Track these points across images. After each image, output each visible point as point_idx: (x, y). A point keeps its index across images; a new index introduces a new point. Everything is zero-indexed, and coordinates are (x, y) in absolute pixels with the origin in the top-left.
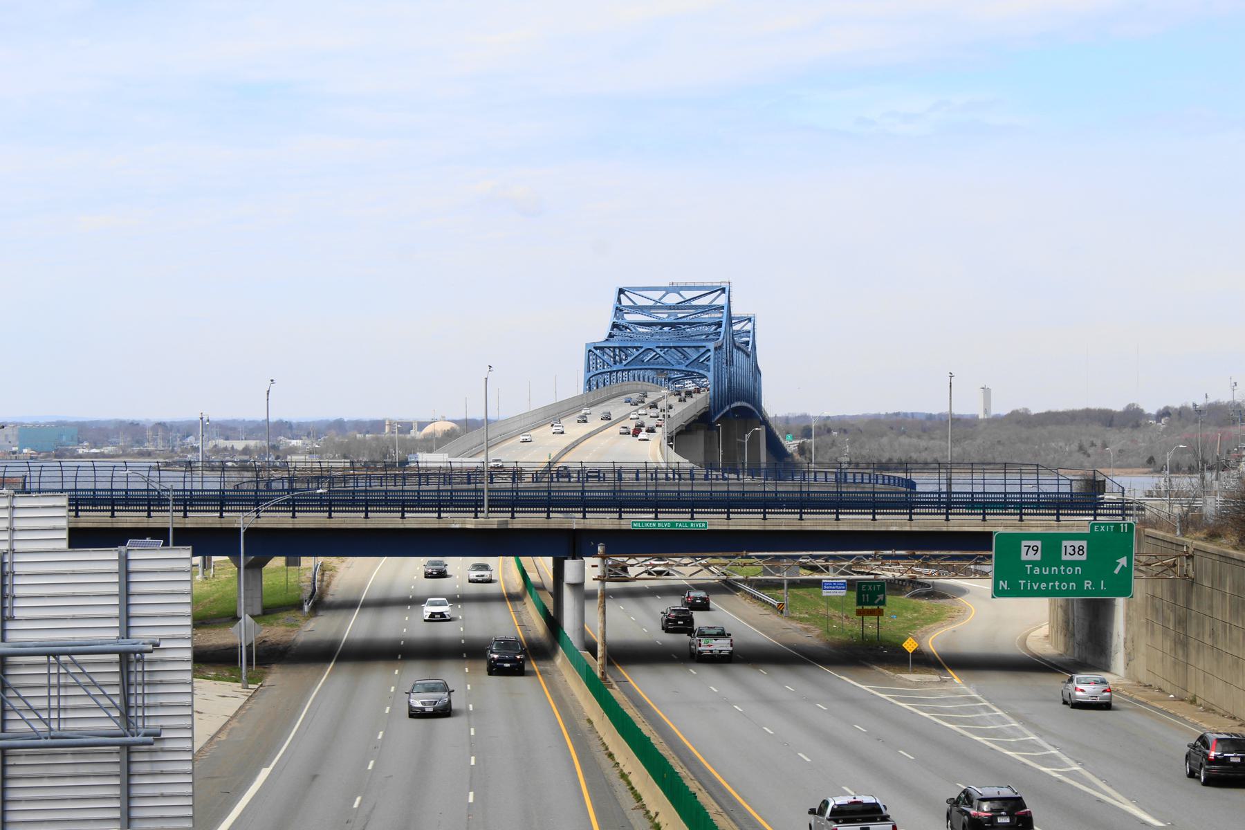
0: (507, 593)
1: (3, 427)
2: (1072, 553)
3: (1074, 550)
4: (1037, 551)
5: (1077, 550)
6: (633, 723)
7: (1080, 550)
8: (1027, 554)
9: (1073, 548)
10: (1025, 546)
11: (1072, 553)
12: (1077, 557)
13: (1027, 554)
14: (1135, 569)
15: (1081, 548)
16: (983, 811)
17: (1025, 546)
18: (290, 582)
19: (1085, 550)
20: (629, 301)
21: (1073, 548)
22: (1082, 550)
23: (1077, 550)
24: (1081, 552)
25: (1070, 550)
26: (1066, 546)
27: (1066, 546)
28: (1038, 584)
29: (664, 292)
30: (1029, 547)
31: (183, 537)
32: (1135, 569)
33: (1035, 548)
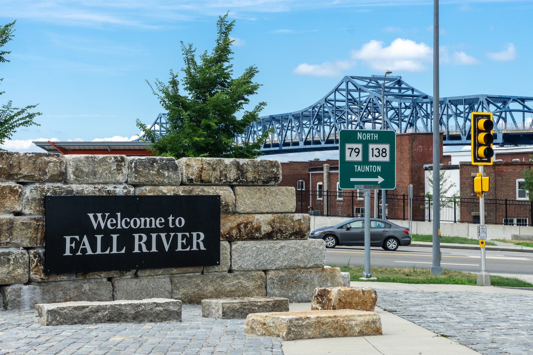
0: (493, 134)
1: (2, 80)
2: (378, 155)
3: (379, 152)
4: (358, 152)
5: (381, 152)
6: (58, 274)
7: (383, 152)
8: (350, 156)
9: (378, 150)
10: (349, 149)
11: (378, 155)
12: (381, 159)
13: (350, 156)
14: (477, 111)
15: (384, 151)
16: (441, 145)
17: (349, 149)
18: (274, 141)
19: (388, 152)
20: (342, 93)
21: (378, 150)
22: (385, 152)
23: (381, 152)
24: (384, 154)
25: (376, 152)
26: (373, 149)
27: (373, 149)
28: (358, 171)
29: (351, 92)
30: (352, 149)
31: (22, 124)
32: (477, 111)
33: (357, 151)
